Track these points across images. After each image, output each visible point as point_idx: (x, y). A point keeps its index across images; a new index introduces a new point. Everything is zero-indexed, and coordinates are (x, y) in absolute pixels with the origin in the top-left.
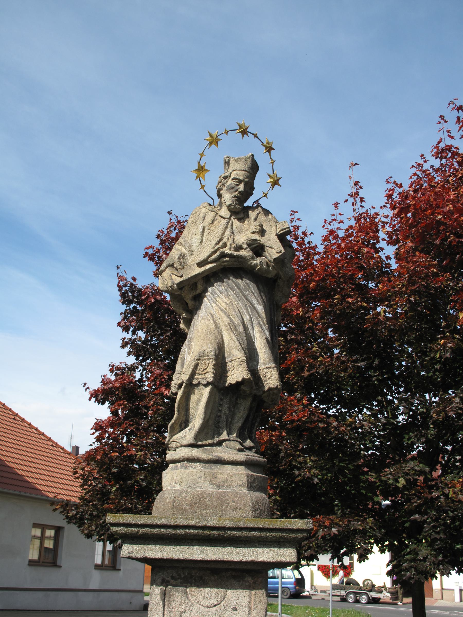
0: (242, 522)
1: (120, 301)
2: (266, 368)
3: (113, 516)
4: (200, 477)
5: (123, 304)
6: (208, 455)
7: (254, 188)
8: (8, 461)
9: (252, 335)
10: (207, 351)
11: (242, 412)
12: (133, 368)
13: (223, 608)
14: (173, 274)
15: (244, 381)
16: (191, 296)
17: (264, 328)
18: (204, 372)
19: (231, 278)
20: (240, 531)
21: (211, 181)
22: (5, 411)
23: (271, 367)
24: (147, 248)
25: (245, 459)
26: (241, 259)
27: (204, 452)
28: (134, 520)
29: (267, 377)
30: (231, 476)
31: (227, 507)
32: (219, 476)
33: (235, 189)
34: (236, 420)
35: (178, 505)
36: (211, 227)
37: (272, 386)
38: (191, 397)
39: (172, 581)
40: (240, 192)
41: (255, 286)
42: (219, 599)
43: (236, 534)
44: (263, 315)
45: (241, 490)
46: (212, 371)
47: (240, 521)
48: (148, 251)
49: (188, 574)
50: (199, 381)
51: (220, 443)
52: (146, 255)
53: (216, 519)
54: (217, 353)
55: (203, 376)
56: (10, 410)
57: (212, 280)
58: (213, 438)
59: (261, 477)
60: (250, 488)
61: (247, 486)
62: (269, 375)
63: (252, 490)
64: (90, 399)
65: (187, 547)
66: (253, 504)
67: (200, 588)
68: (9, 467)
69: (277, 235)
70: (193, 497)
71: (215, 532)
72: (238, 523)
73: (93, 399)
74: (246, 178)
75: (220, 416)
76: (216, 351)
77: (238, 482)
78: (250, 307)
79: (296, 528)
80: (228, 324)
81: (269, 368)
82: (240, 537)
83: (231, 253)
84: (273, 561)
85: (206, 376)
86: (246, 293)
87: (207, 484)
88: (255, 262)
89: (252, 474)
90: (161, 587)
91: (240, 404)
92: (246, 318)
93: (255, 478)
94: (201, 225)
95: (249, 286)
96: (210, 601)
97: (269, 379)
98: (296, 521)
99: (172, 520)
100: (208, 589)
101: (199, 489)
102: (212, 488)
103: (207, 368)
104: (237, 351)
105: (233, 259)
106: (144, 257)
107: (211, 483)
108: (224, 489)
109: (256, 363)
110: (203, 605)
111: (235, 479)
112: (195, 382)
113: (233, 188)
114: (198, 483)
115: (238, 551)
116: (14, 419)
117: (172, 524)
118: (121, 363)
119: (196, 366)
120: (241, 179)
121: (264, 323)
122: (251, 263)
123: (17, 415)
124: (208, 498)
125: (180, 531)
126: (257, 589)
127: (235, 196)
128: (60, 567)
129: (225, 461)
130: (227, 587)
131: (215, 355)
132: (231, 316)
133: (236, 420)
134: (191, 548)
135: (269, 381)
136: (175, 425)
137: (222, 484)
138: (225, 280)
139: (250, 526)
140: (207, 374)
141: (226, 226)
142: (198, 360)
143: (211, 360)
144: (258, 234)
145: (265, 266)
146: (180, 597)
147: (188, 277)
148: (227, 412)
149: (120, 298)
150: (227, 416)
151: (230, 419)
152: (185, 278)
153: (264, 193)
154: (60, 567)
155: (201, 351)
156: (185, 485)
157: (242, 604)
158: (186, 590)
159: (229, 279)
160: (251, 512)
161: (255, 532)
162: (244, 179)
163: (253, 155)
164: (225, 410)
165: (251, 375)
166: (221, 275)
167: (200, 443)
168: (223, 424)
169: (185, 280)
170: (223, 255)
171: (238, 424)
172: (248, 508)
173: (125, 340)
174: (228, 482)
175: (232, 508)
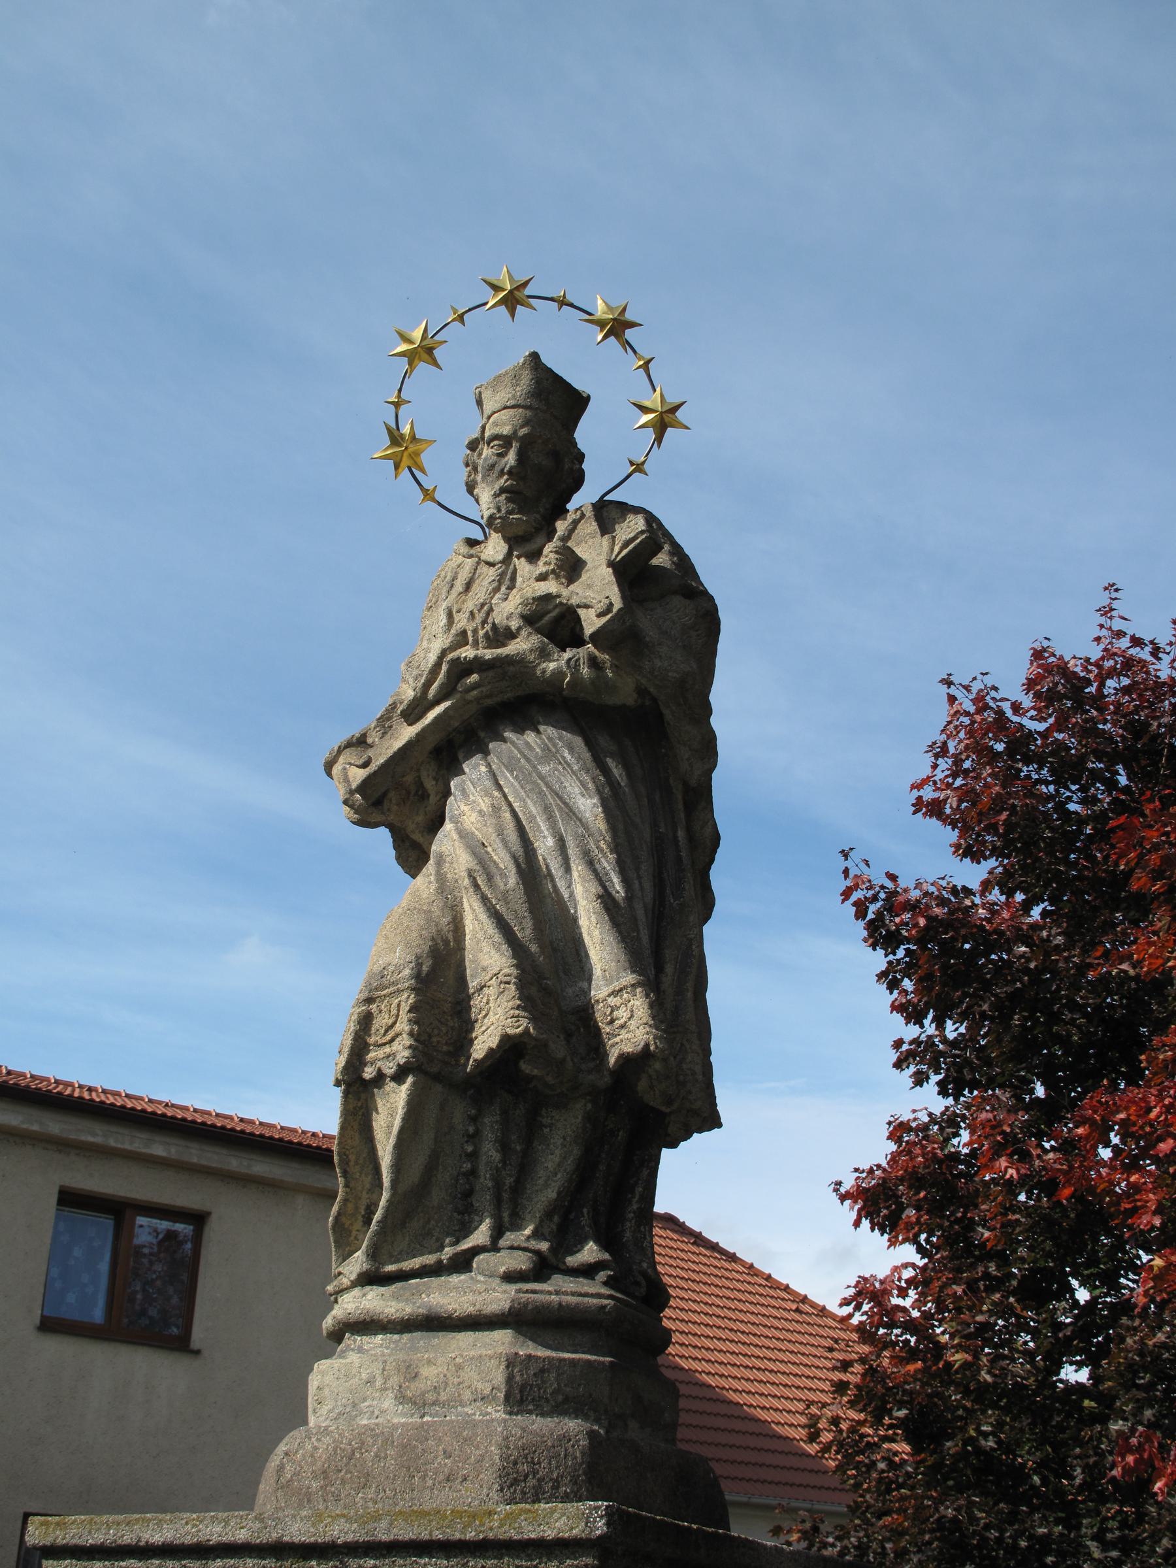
0: (384, 1524)
1: (865, 940)
2: (614, 993)
3: (42, 1525)
4: (370, 1381)
5: (874, 949)
6: (401, 1305)
7: (583, 455)
8: (778, 1423)
9: (566, 896)
10: (391, 968)
11: (558, 1152)
12: (950, 1122)
14: (351, 764)
15: (645, 1054)
16: (420, 818)
17: (606, 865)
18: (388, 1038)
19: (506, 734)
20: (384, 1557)
21: (445, 467)
22: (772, 1292)
23: (625, 987)
24: (915, 786)
25: (507, 1306)
26: (512, 668)
27: (396, 1297)
28: (90, 1532)
29: (618, 1023)
30: (459, 1367)
31: (424, 1478)
32: (425, 1371)
33: (498, 468)
34: (541, 1182)
35: (291, 1480)
36: (464, 602)
37: (628, 1048)
38: (374, 1124)
40: (510, 473)
41: (578, 741)
44: (601, 825)
45: (488, 1414)
46: (407, 1028)
47: (377, 1518)
48: (921, 793)
50: (379, 1070)
51: (462, 1264)
52: (919, 804)
53: (308, 1518)
54: (425, 969)
55: (387, 1049)
56: (787, 1288)
57: (461, 756)
58: (441, 1248)
59: (573, 1362)
60: (521, 1401)
61: (507, 1397)
62: (622, 1014)
63: (530, 1412)
64: (857, 1224)
66: (505, 1458)
68: (780, 1437)
69: (611, 564)
70: (335, 1450)
72: (370, 1527)
73: (866, 1223)
74: (522, 427)
75: (473, 1172)
76: (419, 965)
77: (479, 1386)
78: (560, 809)
79: (550, 1534)
80: (465, 874)
81: (621, 990)
83: (476, 657)
85: (396, 1046)
86: (545, 769)
87: (388, 1403)
88: (552, 666)
89: (529, 1357)
91: (550, 1126)
92: (545, 845)
93: (544, 1368)
94: (444, 605)
95: (555, 745)
97: (622, 1027)
98: (553, 1511)
99: (189, 1526)
101: (365, 1422)
102: (403, 1415)
103: (395, 1023)
104: (493, 952)
105: (491, 674)
106: (915, 813)
107: (401, 1398)
108: (437, 1415)
109: (585, 985)
111: (470, 1374)
112: (369, 1073)
113: (493, 466)
114: (365, 1400)
116: (797, 1310)
117: (188, 1540)
118: (914, 1111)
119: (366, 1021)
120: (505, 433)
121: (601, 850)
122: (544, 671)
123: (805, 1299)
124: (375, 1449)
127: (503, 490)
129: (450, 1317)
131: (417, 976)
132: (489, 849)
133: (541, 1182)
135: (624, 1035)
136: (343, 1219)
137: (430, 1397)
138: (491, 746)
139: (407, 1538)
140: (396, 1042)
141: (496, 584)
142: (369, 1001)
143: (406, 995)
144: (557, 577)
145: (585, 671)
147: (382, 760)
148: (496, 1156)
149: (865, 933)
150: (497, 1169)
151: (509, 1181)
152: (373, 767)
153: (632, 464)
155: (375, 970)
156: (330, 1411)
159: (504, 740)
160: (496, 1487)
161: (431, 1557)
162: (515, 432)
163: (535, 356)
164: (490, 1152)
165: (533, 1019)
166: (482, 734)
167: (390, 1268)
168: (483, 1199)
169: (375, 772)
170: (461, 669)
171: (546, 1190)
172: (489, 1476)
173: (905, 1047)
174: (451, 1389)
175: (441, 1477)
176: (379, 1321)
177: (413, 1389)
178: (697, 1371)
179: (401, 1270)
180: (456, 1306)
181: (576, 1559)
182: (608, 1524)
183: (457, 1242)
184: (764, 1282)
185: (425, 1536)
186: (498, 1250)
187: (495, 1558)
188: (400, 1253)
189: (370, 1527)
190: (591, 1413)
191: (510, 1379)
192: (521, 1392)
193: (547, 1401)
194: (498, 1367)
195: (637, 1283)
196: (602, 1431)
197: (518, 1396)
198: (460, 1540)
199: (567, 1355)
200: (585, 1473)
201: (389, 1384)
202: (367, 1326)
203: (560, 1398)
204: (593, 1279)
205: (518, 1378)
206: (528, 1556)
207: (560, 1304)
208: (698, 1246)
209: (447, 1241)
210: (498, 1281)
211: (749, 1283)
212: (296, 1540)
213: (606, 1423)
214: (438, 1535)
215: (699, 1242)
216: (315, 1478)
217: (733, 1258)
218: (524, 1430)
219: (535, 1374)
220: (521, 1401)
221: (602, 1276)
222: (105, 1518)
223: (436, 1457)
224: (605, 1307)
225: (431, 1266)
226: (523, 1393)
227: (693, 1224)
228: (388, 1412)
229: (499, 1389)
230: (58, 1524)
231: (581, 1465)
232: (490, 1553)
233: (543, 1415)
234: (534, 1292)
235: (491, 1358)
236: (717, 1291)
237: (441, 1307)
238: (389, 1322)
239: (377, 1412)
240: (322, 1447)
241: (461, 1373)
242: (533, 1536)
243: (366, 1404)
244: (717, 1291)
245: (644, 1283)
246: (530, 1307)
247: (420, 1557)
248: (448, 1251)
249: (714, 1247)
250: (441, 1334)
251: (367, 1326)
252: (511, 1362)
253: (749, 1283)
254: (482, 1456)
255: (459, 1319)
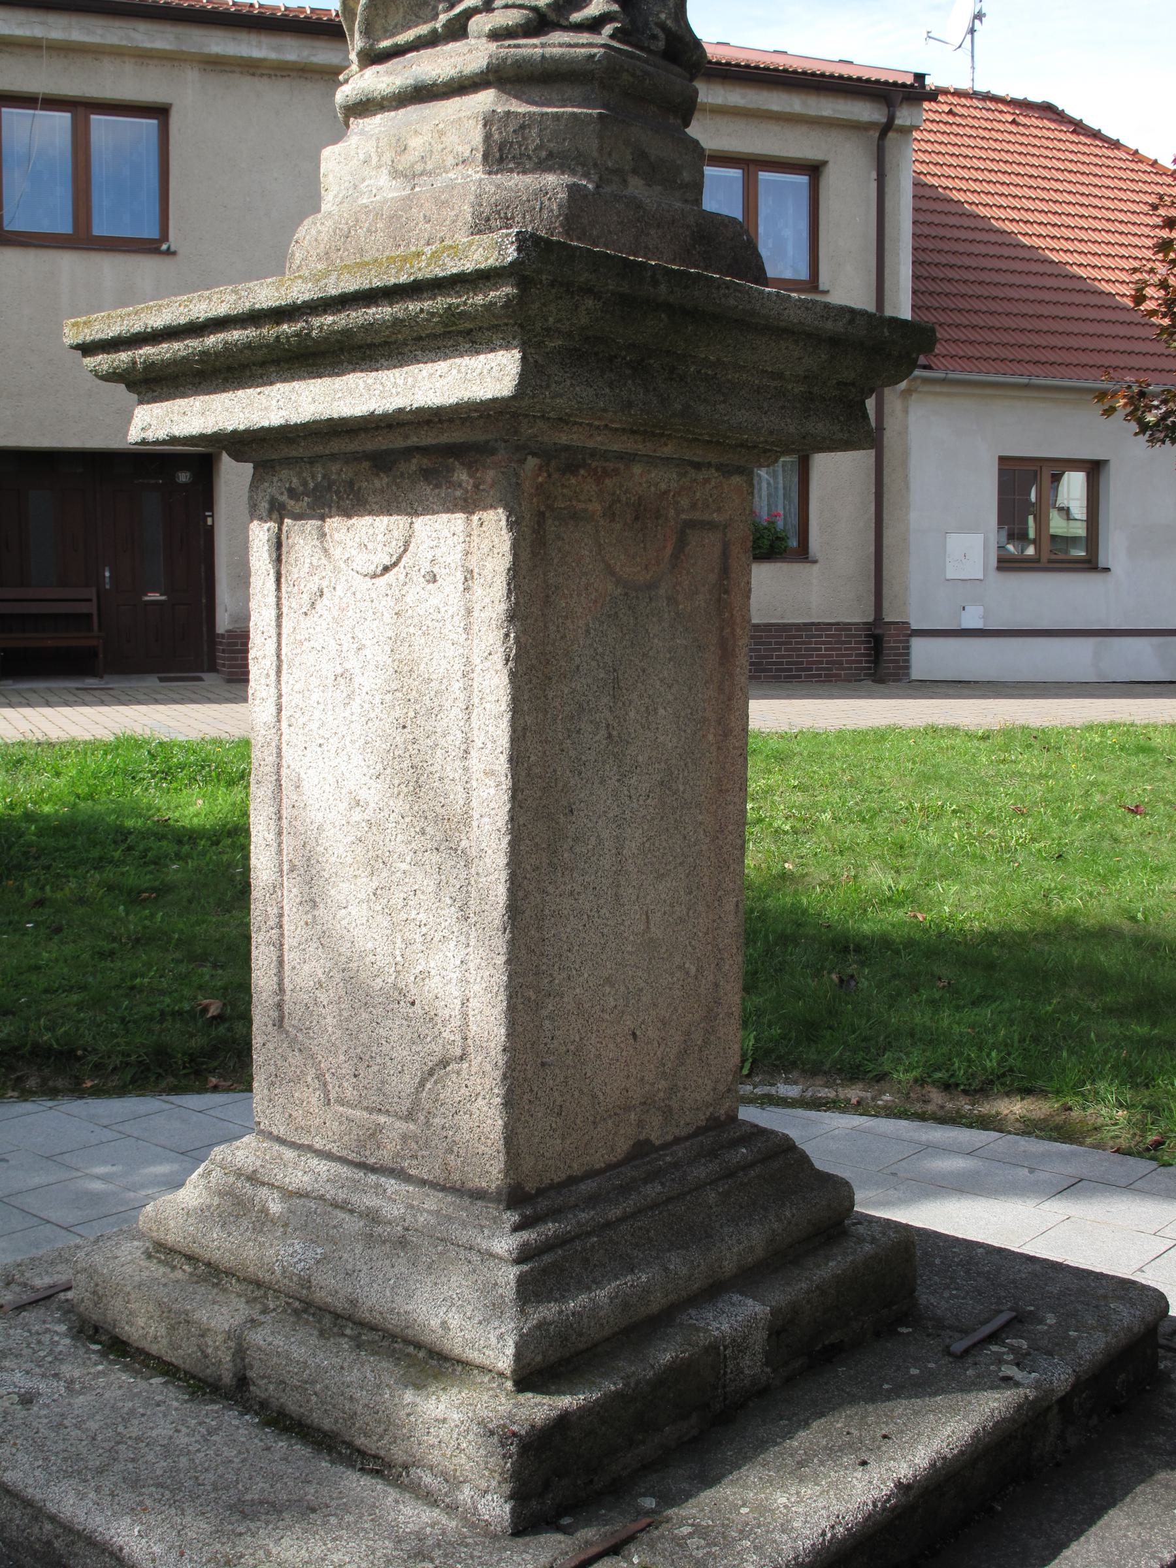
13: (401, 577)
20: (339, 311)
22: (1157, 179)
25: (485, 64)
39: (292, 503)
42: (395, 547)
43: (334, 323)
49: (324, 477)
58: (435, 17)
59: (556, 117)
60: (501, 160)
61: (486, 157)
63: (511, 171)
65: (258, 390)
67: (349, 517)
71: (285, 326)
72: (321, 284)
77: (460, 149)
79: (469, 267)
82: (347, 333)
84: (451, 401)
89: (508, 113)
90: (268, 524)
96: (372, 557)
100: (368, 520)
107: (395, 174)
110: (359, 569)
111: (451, 139)
114: (364, 180)
115: (370, 381)
117: (183, 320)
124: (367, 225)
125: (212, 341)
126: (485, 509)
128: (1107, 570)
129: (434, 84)
130: (413, 510)
134: (267, 390)
137: (419, 168)
139: (352, 289)
146: (307, 551)
154: (1107, 570)
156: (336, 196)
157: (449, 560)
158: (321, 528)
161: (377, 306)
167: (385, 44)
176: (374, 99)
177: (404, 162)
178: (1067, 263)
179: (397, 45)
180: (439, 71)
181: (497, 290)
182: (519, 250)
183: (452, 6)
184: (1149, 169)
185: (366, 285)
186: (493, 10)
187: (430, 299)
188: (395, 26)
189: (321, 284)
190: (579, 169)
191: (488, 138)
192: (500, 150)
193: (529, 157)
194: (475, 128)
195: (654, 37)
196: (590, 186)
197: (497, 155)
198: (395, 284)
199: (549, 110)
200: (562, 225)
201: (383, 159)
202: (364, 107)
203: (544, 154)
204: (600, 34)
205: (496, 136)
206: (457, 292)
207: (543, 56)
208: (1078, 134)
209: (440, 7)
210: (484, 40)
211: (1132, 170)
212: (265, 306)
213: (595, 178)
214: (377, 283)
215: (1079, 130)
216: (320, 259)
217: (1116, 145)
218: (498, 187)
219: (514, 131)
220: (501, 160)
221: (608, 29)
222: (119, 311)
223: (417, 224)
224: (595, 55)
225: (425, 36)
226: (501, 153)
227: (1092, 122)
228: (384, 188)
229: (476, 150)
230: (85, 323)
231: (557, 217)
232: (425, 295)
233: (524, 172)
234: (518, 46)
235: (469, 118)
236: (1096, 181)
237: (426, 74)
238: (383, 98)
239: (374, 191)
240: (324, 229)
241: (444, 139)
242: (455, 271)
243: (365, 184)
244: (1096, 181)
245: (662, 35)
246: (509, 61)
247: (369, 307)
248: (443, 18)
249: (1096, 135)
250: (431, 104)
251: (364, 107)
252: (489, 121)
253: (1132, 170)
254: (457, 216)
255: (445, 84)
